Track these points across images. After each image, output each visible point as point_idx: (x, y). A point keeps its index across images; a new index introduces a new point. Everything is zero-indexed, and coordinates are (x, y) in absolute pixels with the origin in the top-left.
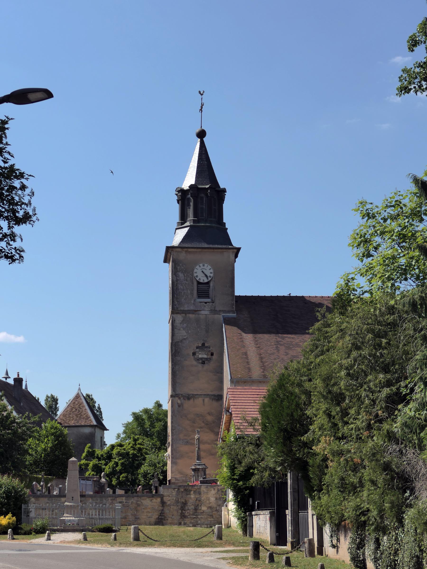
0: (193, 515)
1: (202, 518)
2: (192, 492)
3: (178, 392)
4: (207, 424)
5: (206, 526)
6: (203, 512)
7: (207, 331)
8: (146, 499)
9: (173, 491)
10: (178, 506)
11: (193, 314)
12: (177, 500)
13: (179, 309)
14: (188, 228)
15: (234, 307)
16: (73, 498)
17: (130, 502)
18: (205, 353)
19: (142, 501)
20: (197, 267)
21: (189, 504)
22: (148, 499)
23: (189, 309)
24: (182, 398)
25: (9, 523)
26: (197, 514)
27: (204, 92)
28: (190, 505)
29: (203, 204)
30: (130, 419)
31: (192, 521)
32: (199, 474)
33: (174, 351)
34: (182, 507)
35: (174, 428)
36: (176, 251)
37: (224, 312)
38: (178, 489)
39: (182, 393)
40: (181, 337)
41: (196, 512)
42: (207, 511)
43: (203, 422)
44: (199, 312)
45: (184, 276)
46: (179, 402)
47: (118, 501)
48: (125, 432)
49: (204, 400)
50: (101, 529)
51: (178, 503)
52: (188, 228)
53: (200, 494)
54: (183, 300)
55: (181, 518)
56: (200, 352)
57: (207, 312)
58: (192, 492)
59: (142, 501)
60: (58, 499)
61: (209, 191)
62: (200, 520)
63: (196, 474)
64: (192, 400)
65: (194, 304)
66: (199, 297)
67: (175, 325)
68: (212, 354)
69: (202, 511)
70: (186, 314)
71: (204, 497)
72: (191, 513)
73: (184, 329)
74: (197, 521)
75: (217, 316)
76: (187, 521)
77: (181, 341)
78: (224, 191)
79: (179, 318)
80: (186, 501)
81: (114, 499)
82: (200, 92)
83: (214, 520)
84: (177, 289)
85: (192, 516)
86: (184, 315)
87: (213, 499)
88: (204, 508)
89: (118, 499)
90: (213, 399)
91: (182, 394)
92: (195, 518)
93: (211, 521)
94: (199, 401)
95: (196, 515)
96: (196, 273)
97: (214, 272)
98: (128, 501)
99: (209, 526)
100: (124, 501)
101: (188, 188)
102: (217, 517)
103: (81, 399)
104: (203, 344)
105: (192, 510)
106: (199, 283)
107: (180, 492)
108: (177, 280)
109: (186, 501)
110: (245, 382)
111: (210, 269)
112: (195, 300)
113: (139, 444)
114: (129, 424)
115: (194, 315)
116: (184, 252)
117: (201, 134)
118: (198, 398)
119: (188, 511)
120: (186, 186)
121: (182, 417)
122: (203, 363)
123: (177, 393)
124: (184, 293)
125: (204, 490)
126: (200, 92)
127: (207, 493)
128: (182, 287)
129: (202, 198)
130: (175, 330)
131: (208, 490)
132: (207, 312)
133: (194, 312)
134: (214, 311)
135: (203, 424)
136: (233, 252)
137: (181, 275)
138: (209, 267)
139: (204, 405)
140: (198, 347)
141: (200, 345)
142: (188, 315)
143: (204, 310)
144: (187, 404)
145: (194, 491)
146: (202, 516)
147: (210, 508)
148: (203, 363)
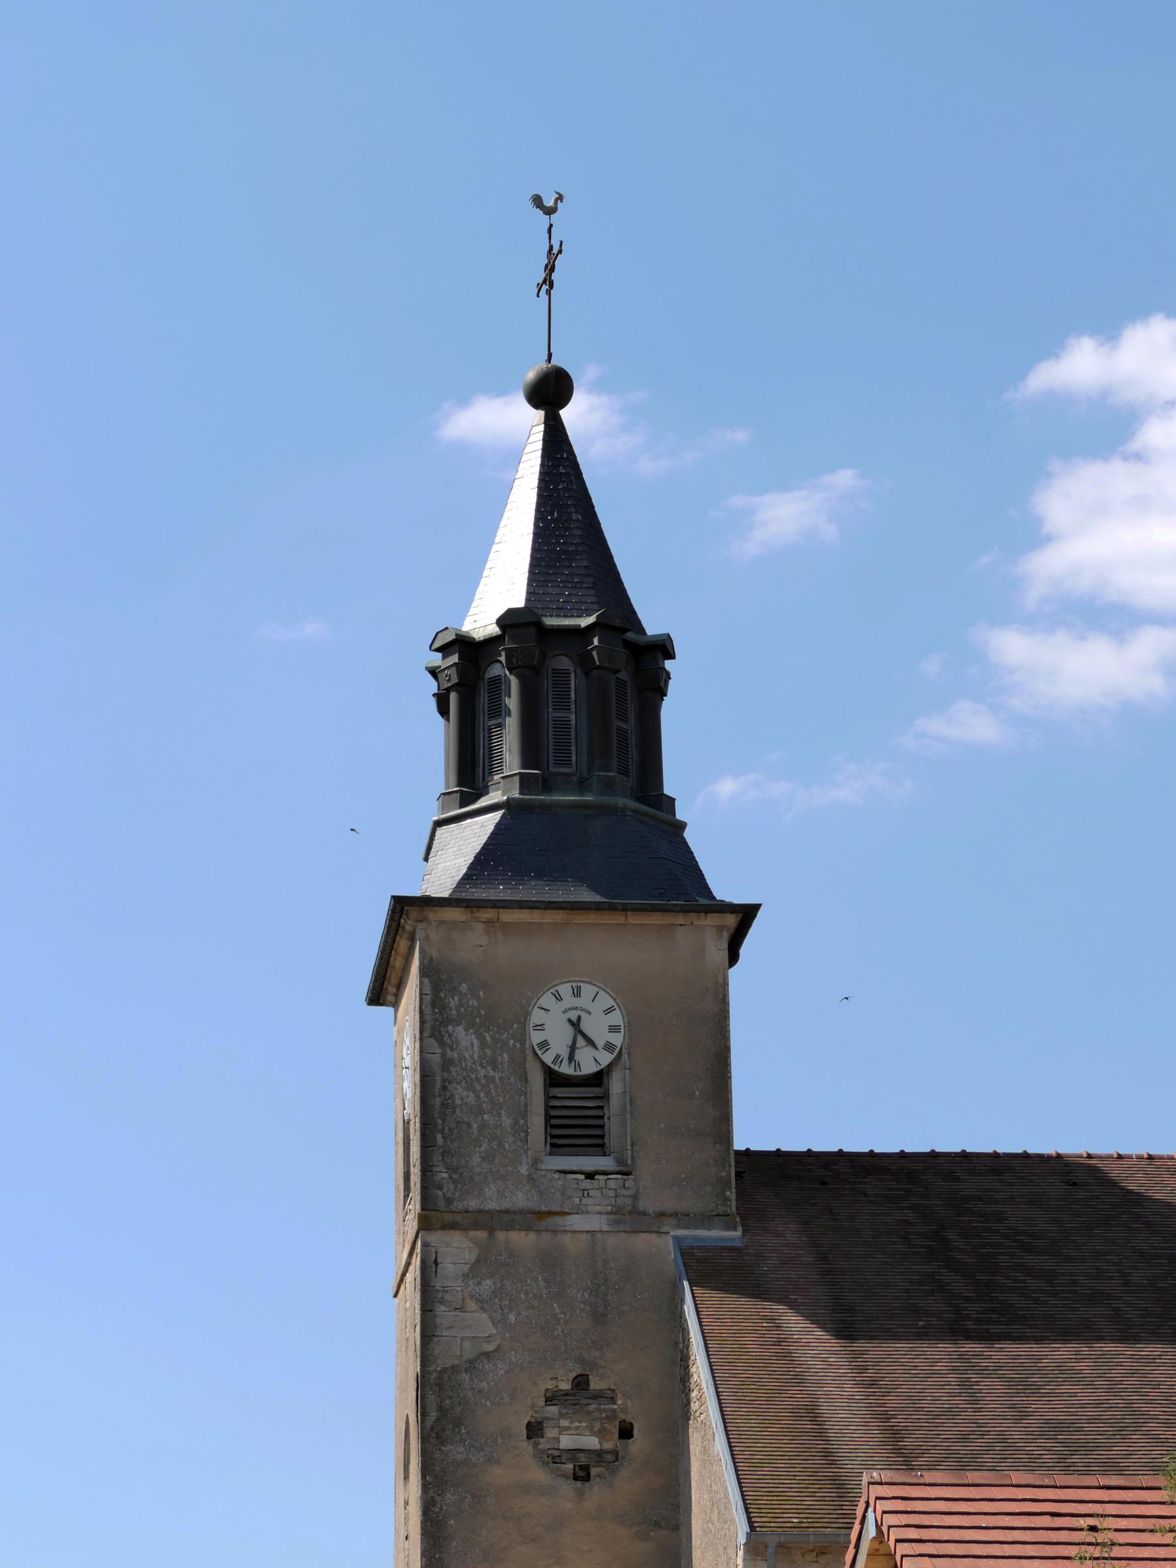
7: (599, 1317)
11: (529, 1229)
13: (459, 1206)
14: (496, 816)
15: (732, 1194)
23: (506, 1205)
27: (560, 198)
29: (566, 701)
33: (433, 1416)
37: (683, 1218)
40: (467, 1345)
44: (559, 1220)
45: (483, 1044)
52: (496, 816)
54: (476, 1159)
56: (564, 1423)
57: (596, 1223)
61: (596, 641)
65: (530, 1178)
66: (556, 1146)
67: (438, 1284)
68: (626, 1432)
70: (491, 1231)
73: (483, 1304)
75: (643, 1242)
77: (471, 1366)
79: (458, 1250)
82: (538, 201)
86: (481, 1234)
96: (540, 1027)
97: (629, 1026)
104: (581, 1382)
106: (553, 1079)
108: (446, 1064)
112: (535, 1163)
115: (532, 1236)
116: (480, 927)
120: (481, 621)
122: (582, 1475)
124: (484, 1126)
126: (538, 201)
128: (471, 1099)
129: (561, 677)
134: (630, 1217)
136: (720, 928)
137: (464, 1037)
138: (606, 1001)
140: (551, 1398)
141: (565, 1386)
142: (501, 1235)
143: (579, 1211)
148: (582, 1475)
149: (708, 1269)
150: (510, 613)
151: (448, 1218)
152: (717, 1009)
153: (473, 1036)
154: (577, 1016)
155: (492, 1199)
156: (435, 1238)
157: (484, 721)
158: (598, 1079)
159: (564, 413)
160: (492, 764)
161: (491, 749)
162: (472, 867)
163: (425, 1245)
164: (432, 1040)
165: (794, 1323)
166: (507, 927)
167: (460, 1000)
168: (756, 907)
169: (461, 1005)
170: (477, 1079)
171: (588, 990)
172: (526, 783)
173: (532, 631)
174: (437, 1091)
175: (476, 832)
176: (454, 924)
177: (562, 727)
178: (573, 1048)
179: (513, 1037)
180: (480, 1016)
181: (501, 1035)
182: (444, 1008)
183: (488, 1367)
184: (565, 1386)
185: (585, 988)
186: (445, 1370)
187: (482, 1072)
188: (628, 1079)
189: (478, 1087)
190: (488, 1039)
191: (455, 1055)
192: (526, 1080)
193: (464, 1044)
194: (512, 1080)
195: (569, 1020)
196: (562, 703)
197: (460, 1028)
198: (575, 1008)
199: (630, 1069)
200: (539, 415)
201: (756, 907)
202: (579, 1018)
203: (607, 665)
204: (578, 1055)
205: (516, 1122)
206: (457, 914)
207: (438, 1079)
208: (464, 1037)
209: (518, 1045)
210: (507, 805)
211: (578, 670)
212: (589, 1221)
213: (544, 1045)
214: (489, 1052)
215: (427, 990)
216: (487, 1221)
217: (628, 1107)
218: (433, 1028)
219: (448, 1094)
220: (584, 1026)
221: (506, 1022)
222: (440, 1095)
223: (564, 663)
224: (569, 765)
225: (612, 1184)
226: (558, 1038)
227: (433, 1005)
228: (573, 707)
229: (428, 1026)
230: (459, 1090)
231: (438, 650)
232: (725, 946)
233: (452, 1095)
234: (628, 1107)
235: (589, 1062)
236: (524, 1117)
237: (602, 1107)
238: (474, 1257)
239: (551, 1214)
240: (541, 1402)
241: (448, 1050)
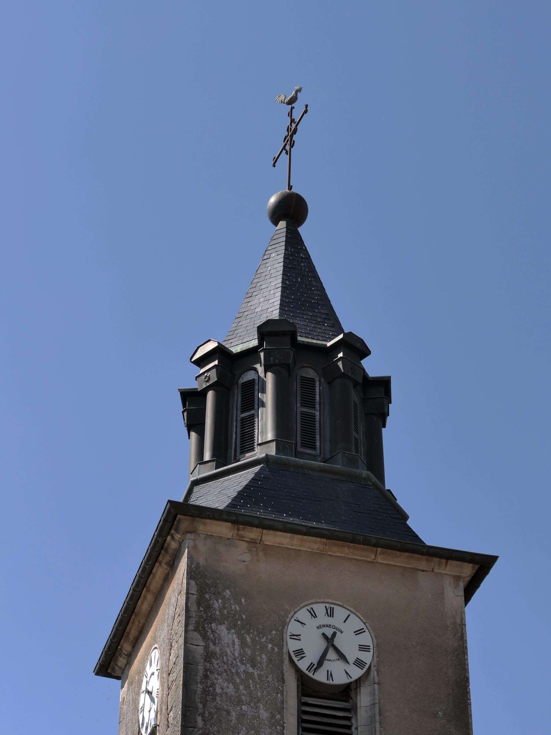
20: (314, 606)
45: (243, 644)
78: (384, 384)
84: (205, 691)
96: (296, 637)
97: (378, 646)
101: (255, 343)
106: (307, 686)
108: (209, 656)
111: (359, 632)
116: (243, 546)
117: (291, 210)
128: (231, 689)
129: (308, 384)
136: (457, 578)
137: (226, 636)
138: (356, 623)
150: (269, 322)
152: (456, 644)
153: (235, 636)
154: (332, 629)
158: (347, 692)
159: (301, 230)
164: (195, 633)
166: (267, 549)
167: (224, 603)
168: (493, 559)
169: (224, 607)
170: (237, 673)
171: (340, 613)
173: (288, 339)
174: (199, 679)
176: (220, 539)
177: (308, 420)
179: (271, 641)
180: (242, 620)
181: (260, 638)
182: (209, 607)
185: (337, 609)
187: (242, 668)
188: (377, 693)
189: (238, 681)
190: (249, 640)
191: (217, 649)
192: (283, 681)
193: (226, 641)
194: (270, 679)
195: (324, 634)
196: (308, 401)
197: (223, 627)
198: (329, 626)
199: (379, 684)
201: (493, 559)
202: (334, 634)
203: (350, 374)
205: (273, 716)
206: (223, 529)
207: (201, 668)
208: (226, 636)
209: (276, 649)
210: (267, 460)
211: (322, 380)
213: (300, 653)
214: (249, 652)
215: (194, 590)
217: (377, 717)
218: (197, 623)
219: (209, 683)
221: (266, 627)
222: (201, 683)
223: (310, 373)
224: (314, 448)
227: (199, 604)
228: (317, 406)
229: (193, 621)
230: (220, 681)
232: (462, 593)
233: (213, 685)
234: (377, 717)
235: (338, 673)
236: (281, 712)
237: (348, 719)
241: (211, 644)
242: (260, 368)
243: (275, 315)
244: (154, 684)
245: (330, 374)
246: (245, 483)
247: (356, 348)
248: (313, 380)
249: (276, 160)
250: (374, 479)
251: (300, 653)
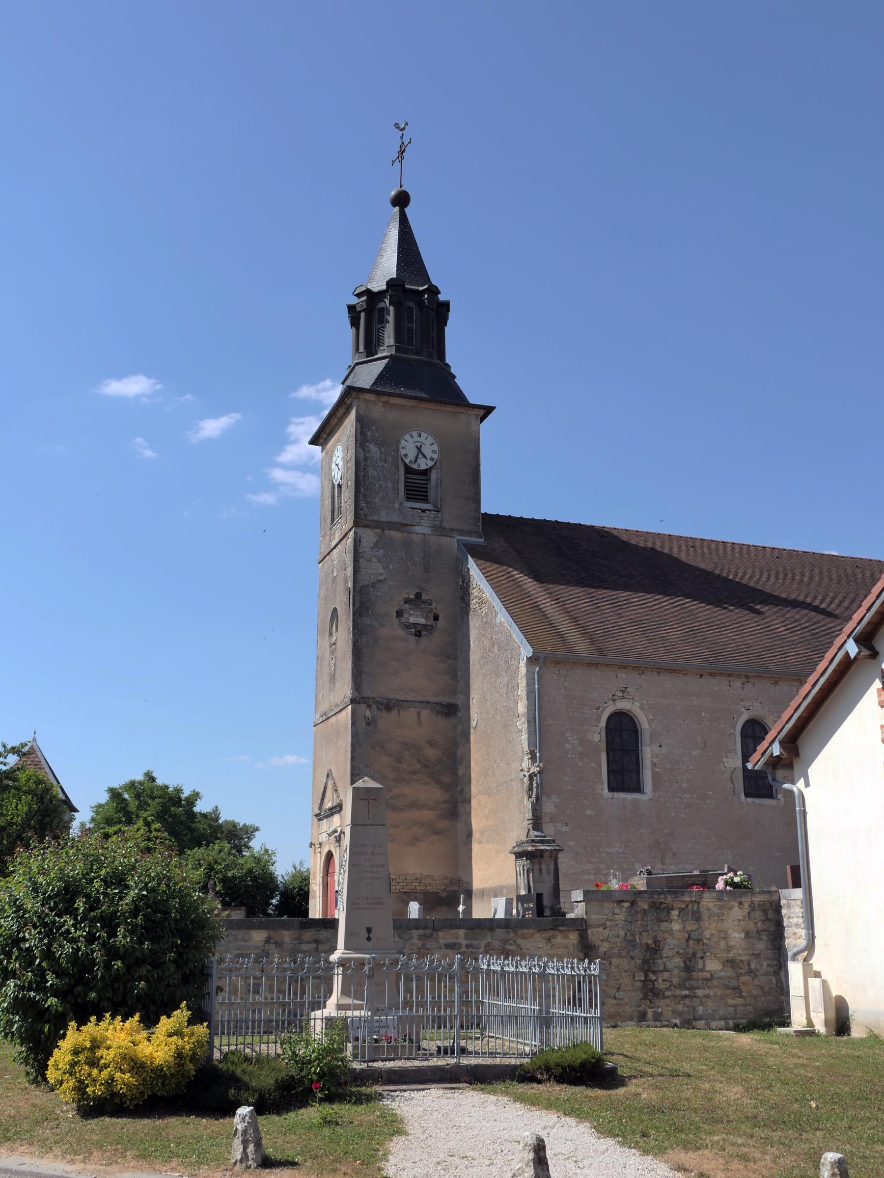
0: (682, 986)
1: (707, 996)
2: (676, 912)
3: (367, 693)
4: (426, 766)
5: (722, 1023)
6: (712, 977)
7: (426, 570)
8: (532, 935)
9: (617, 911)
10: (632, 958)
11: (398, 530)
12: (629, 938)
13: (370, 518)
14: (386, 361)
15: (480, 524)
16: (369, 930)
17: (483, 944)
18: (422, 615)
19: (520, 941)
21: (666, 952)
22: (538, 936)
23: (389, 520)
24: (374, 707)
25: (179, 1055)
26: (693, 983)
27: (407, 124)
28: (670, 954)
29: (406, 322)
30: (104, 798)
31: (680, 1008)
32: (544, 866)
33: (358, 605)
34: (645, 961)
35: (356, 772)
36: (365, 400)
37: (461, 532)
38: (633, 903)
39: (374, 696)
40: (372, 576)
41: (690, 978)
42: (722, 974)
43: (418, 760)
44: (411, 528)
45: (381, 452)
46: (368, 714)
47: (442, 941)
48: (93, 820)
49: (419, 714)
50: (572, 1068)
51: (634, 946)
52: (386, 361)
53: (697, 917)
54: (377, 499)
55: (645, 997)
56: (412, 612)
57: (426, 530)
58: (676, 912)
59: (520, 941)
60: (241, 933)
61: (426, 296)
62: (702, 1004)
63: (537, 867)
64: (394, 713)
65: (399, 509)
66: (409, 498)
67: (360, 550)
68: (436, 618)
69: (708, 975)
70: (383, 530)
71: (709, 929)
72: (675, 981)
73: (379, 560)
74: (694, 1009)
75: (445, 540)
76: (664, 1006)
77: (374, 585)
78: (446, 306)
79: (369, 536)
80: (656, 941)
81: (430, 936)
82: (397, 126)
83: (746, 1005)
84: (365, 476)
85: (678, 992)
86: (379, 531)
87: (737, 936)
88: (713, 965)
89: (441, 934)
90: (438, 713)
91: (373, 698)
92: (686, 996)
93: (735, 1006)
94: (410, 715)
95: (692, 988)
96: (404, 448)
97: (440, 451)
98: (475, 943)
99: (731, 1023)
100: (464, 942)
101: (384, 287)
102: (755, 992)
103: (37, 756)
104: (418, 596)
105: (676, 972)
106: (409, 470)
107: (637, 912)
108: (366, 459)
109: (656, 941)
110: (558, 663)
111: (432, 444)
112: (401, 504)
113: (155, 830)
114: (100, 806)
115: (399, 534)
116: (381, 404)
117: (401, 200)
118: (408, 708)
119: (666, 975)
120: (378, 285)
121: (373, 748)
122: (418, 634)
123: (364, 694)
124: (380, 486)
125: (711, 905)
126: (397, 126)
127: (720, 917)
128: (375, 474)
129: (410, 310)
130: (361, 560)
131: (721, 908)
132: (426, 530)
133: (400, 526)
134: (440, 530)
135: (418, 766)
136: (477, 416)
137: (373, 448)
138: (431, 440)
139: (420, 723)
140: (406, 601)
141: (412, 597)
142: (387, 532)
143: (419, 524)
144: (386, 720)
145: (681, 910)
146: (707, 992)
147: (731, 963)
148: (418, 634)
149: (479, 553)
151: (366, 522)
154: (419, 446)
155: (383, 516)
156: (360, 531)
157: (376, 326)
158: (426, 472)
160: (379, 342)
161: (379, 337)
162: (376, 379)
163: (355, 533)
165: (517, 575)
166: (393, 406)
168: (493, 408)
172: (397, 349)
175: (377, 367)
177: (410, 330)
178: (417, 458)
182: (365, 435)
183: (381, 586)
184: (412, 597)
186: (363, 586)
196: (410, 320)
200: (397, 209)
201: (493, 408)
204: (419, 461)
206: (371, 397)
208: (373, 448)
212: (423, 529)
213: (406, 455)
216: (382, 526)
220: (422, 450)
221: (390, 444)
223: (411, 304)
225: (432, 515)
226: (411, 453)
231: (356, 295)
235: (423, 464)
238: (376, 540)
239: (407, 525)
240: (402, 603)
242: (387, 302)
243: (395, 276)
244: (340, 462)
245: (421, 305)
246: (381, 369)
247: (434, 291)
248: (412, 308)
249: (393, 162)
250: (441, 363)
251: (406, 455)
